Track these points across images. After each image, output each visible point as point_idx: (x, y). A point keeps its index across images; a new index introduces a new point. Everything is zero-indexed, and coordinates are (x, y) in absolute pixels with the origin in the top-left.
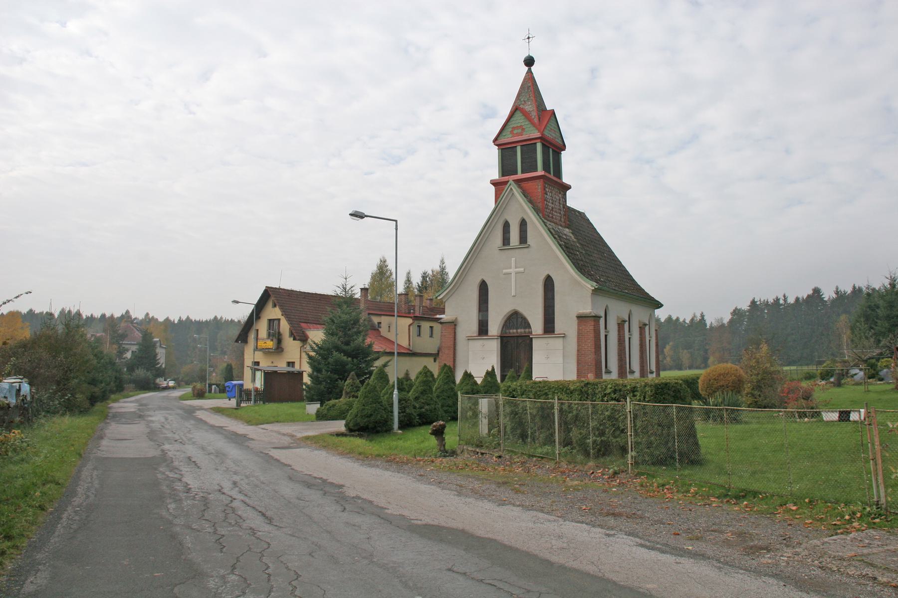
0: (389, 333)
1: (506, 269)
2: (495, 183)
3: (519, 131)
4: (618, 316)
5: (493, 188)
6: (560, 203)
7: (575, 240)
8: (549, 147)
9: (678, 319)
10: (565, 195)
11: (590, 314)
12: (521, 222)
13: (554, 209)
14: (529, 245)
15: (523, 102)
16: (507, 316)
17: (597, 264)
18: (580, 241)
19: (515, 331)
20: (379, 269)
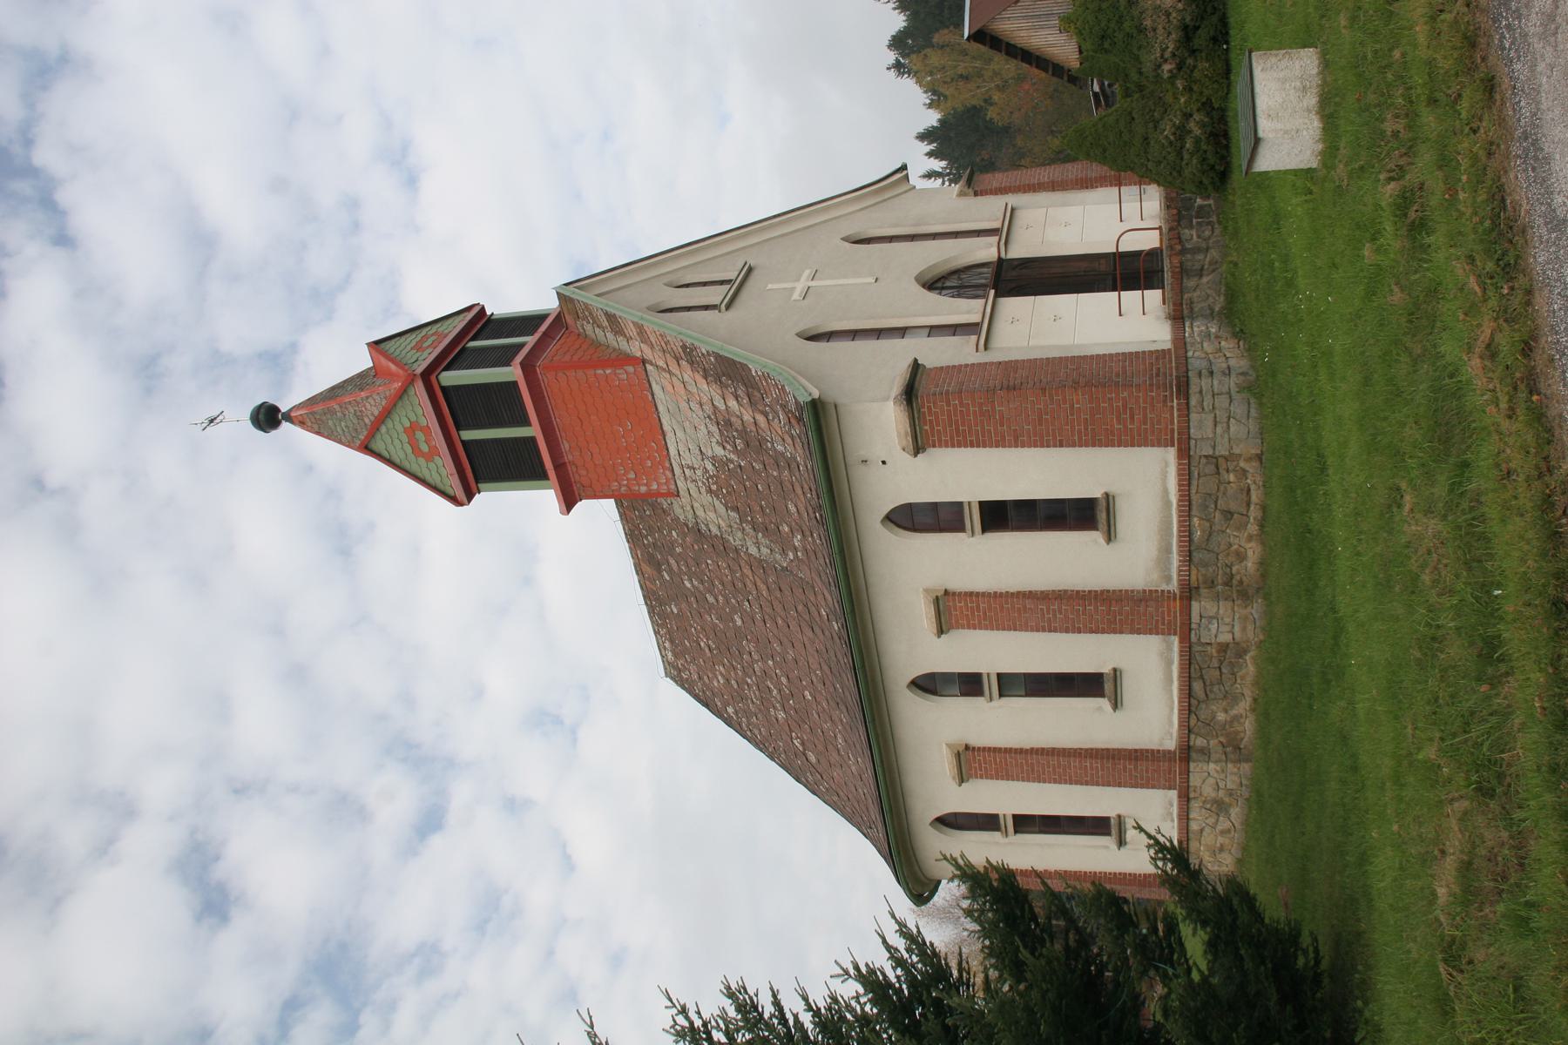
8: (464, 349)
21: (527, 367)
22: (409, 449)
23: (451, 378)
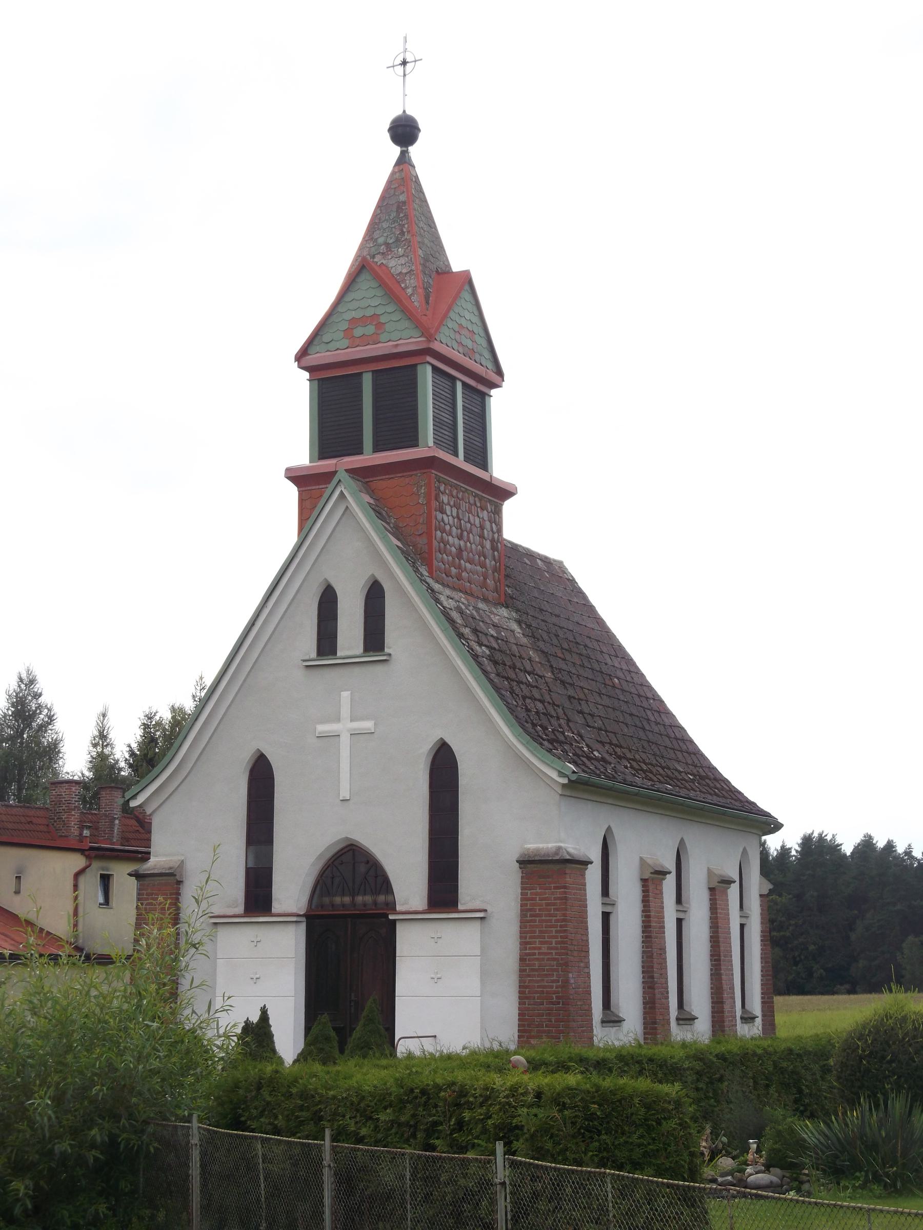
0: (17, 899)
1: (323, 722)
2: (297, 477)
3: (370, 329)
4: (641, 859)
5: (292, 492)
6: (482, 536)
7: (524, 641)
8: (453, 379)
9: (890, 846)
10: (498, 512)
11: (556, 853)
12: (372, 585)
13: (465, 554)
14: (390, 655)
15: (383, 248)
16: (329, 855)
17: (586, 710)
18: (541, 644)
19: (347, 900)
20: (13, 705)
21: (430, 463)
22: (358, 314)
23: (427, 379)
